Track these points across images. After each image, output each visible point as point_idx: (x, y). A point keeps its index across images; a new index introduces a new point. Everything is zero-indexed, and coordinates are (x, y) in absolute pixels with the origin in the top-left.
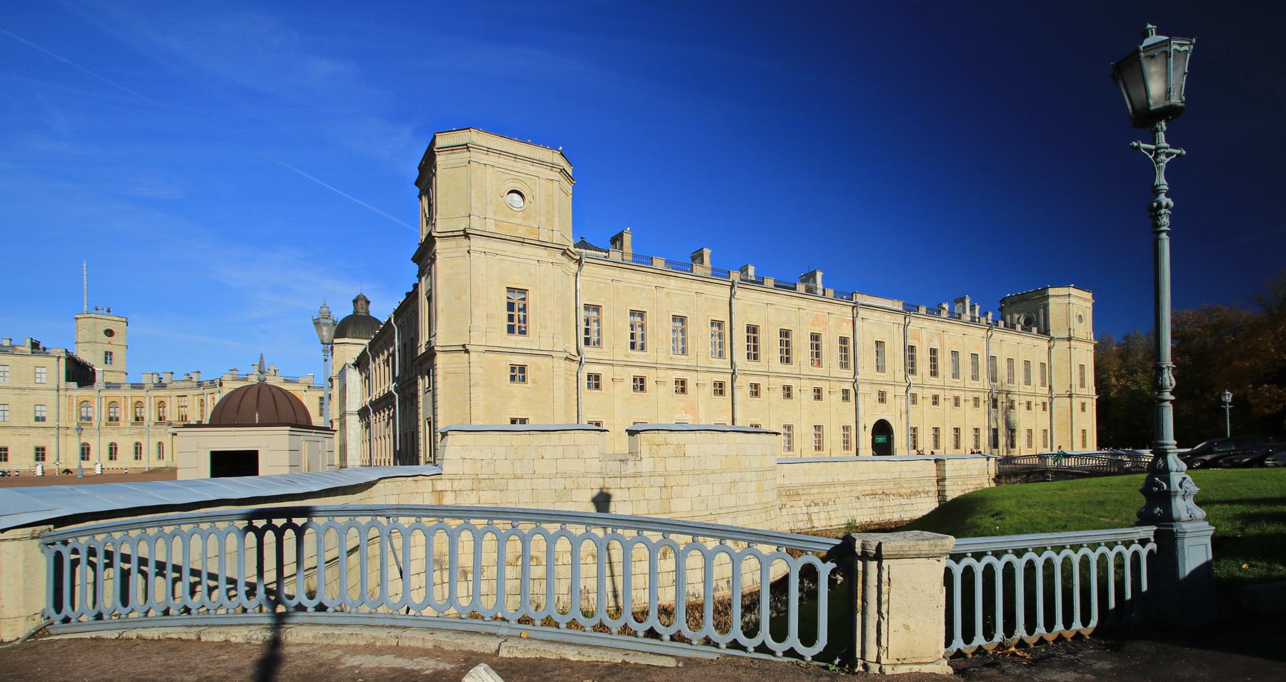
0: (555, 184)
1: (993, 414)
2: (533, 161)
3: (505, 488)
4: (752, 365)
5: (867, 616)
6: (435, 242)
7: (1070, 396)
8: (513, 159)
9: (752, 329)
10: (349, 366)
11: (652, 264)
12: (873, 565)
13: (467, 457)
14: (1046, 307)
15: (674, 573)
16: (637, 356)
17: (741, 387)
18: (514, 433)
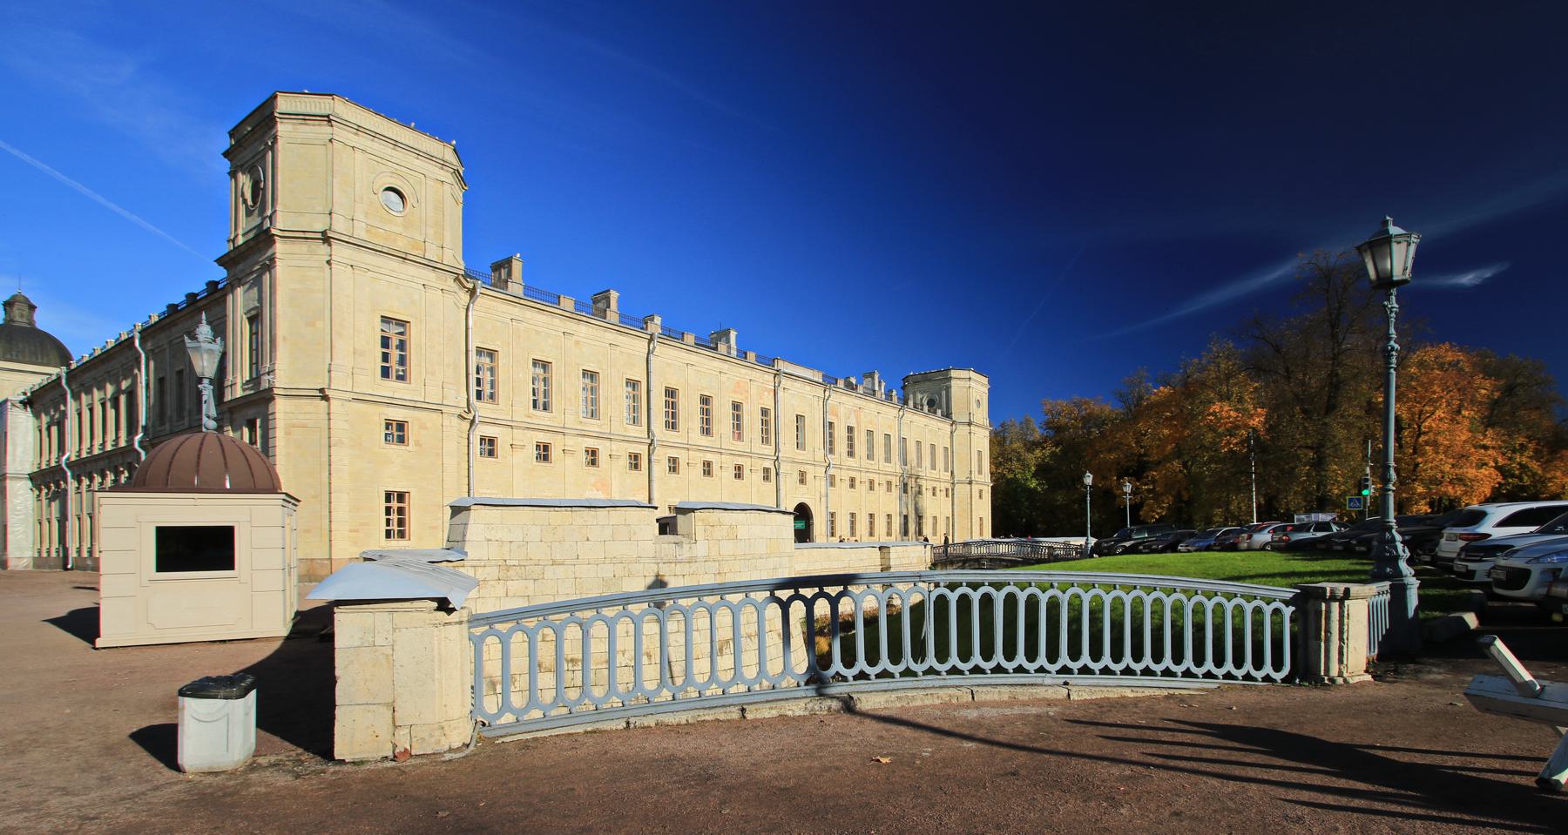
0: (447, 187)
1: (904, 499)
2: (418, 153)
3: (541, 576)
4: (671, 436)
5: (1331, 643)
6: (274, 242)
7: (970, 483)
8: (392, 146)
9: (671, 393)
10: (13, 405)
11: (559, 305)
12: (1335, 606)
13: (492, 538)
14: (948, 389)
15: (733, 670)
16: (541, 417)
17: (659, 461)
18: (552, 509)
